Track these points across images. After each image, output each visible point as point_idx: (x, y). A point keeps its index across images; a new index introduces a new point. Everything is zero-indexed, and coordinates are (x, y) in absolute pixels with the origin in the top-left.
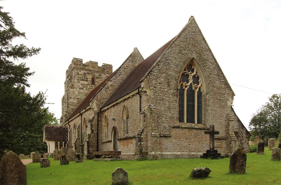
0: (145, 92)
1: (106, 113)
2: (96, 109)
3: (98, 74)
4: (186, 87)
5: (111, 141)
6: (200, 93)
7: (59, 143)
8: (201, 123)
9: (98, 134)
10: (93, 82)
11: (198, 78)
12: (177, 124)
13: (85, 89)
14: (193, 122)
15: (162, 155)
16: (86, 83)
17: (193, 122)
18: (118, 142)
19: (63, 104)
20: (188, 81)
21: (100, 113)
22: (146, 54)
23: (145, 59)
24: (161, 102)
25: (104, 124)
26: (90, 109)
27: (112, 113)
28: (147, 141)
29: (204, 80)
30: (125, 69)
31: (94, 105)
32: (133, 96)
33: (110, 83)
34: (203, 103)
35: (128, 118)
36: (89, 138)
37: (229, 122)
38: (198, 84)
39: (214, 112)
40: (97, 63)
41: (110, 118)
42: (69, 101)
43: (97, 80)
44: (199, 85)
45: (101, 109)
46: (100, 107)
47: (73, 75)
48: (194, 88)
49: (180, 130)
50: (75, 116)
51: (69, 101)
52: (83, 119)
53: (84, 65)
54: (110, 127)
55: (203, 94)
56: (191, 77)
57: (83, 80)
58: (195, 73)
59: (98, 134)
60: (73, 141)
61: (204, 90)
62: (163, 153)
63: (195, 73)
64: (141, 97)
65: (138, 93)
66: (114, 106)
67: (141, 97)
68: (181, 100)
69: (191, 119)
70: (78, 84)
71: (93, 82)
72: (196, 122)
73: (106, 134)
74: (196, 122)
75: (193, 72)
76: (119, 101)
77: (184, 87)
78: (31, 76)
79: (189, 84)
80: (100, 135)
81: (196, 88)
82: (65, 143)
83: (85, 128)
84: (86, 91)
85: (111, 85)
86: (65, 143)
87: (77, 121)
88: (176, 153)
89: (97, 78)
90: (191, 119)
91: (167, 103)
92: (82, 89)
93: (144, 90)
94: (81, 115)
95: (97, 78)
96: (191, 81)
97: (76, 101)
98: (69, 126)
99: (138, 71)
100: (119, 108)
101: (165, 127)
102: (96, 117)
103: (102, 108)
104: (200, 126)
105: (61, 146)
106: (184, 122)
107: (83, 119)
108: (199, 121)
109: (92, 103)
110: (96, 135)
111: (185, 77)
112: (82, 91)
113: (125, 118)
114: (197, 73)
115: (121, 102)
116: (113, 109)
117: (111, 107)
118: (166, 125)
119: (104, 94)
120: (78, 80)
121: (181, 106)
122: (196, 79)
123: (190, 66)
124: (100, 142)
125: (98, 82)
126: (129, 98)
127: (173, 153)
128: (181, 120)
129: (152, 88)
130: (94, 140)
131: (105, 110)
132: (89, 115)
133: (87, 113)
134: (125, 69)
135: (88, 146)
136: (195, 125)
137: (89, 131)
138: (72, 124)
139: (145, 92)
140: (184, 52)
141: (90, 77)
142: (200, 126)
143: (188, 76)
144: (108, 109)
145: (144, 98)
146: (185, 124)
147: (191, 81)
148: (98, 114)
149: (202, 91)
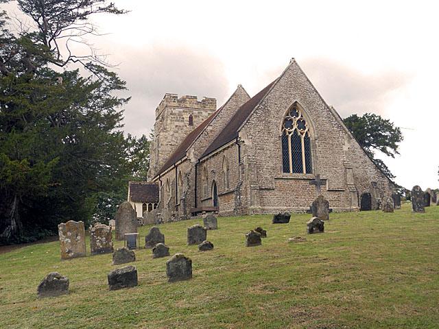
0: (244, 142)
1: (205, 165)
2: (193, 160)
3: (197, 112)
4: (290, 133)
5: (219, 196)
6: (307, 139)
7: (147, 205)
8: (311, 173)
9: (196, 190)
10: (191, 123)
11: (304, 122)
12: (282, 175)
13: (180, 132)
14: (301, 171)
15: (264, 210)
16: (182, 124)
17: (301, 171)
18: (219, 198)
19: (24, 243)
20: (292, 127)
21: (199, 164)
22: (252, 92)
23: (251, 97)
24: (261, 151)
25: (203, 178)
26: (186, 159)
27: (211, 164)
28: (246, 195)
29: (310, 124)
30: (227, 110)
31: (192, 155)
32: (232, 145)
33: (210, 128)
34: (312, 149)
35: (228, 170)
36: (185, 196)
37: (346, 171)
38: (304, 128)
39: (326, 160)
40: (195, 98)
41: (209, 170)
42: (160, 149)
43: (194, 120)
44: (306, 130)
45: (199, 160)
46: (199, 158)
47: (166, 115)
48: (299, 134)
49: (285, 181)
50: (169, 169)
51: (160, 149)
52: (178, 173)
53: (178, 101)
54: (210, 181)
55: (311, 139)
56: (295, 122)
57: (178, 121)
58: (299, 117)
59: (196, 190)
60: (166, 202)
61: (312, 135)
62: (265, 208)
63: (299, 117)
64: (239, 147)
65: (236, 143)
66: (213, 156)
67: (239, 147)
68: (285, 148)
69: (298, 169)
70: (171, 125)
71: (191, 123)
72: (291, 170)
73: (206, 191)
74: (305, 172)
75: (297, 116)
76: (218, 151)
77: (288, 134)
78: (130, 100)
79: (293, 129)
80: (198, 191)
81: (302, 134)
82: (156, 205)
83: (180, 184)
84: (182, 135)
85: (211, 131)
86: (156, 205)
87: (171, 175)
88: (281, 207)
89: (196, 116)
90: (298, 169)
91: (268, 152)
92: (177, 132)
93: (242, 140)
94: (176, 167)
95: (196, 116)
96: (295, 127)
97: (169, 148)
98: (160, 182)
99: (247, 109)
100: (220, 158)
101: (266, 179)
102: (194, 170)
103: (201, 158)
104: (310, 176)
105: (150, 209)
106: (289, 172)
107: (178, 173)
108: (309, 171)
109: (189, 154)
110: (194, 191)
111: (287, 123)
112: (176, 135)
113: (225, 169)
114: (302, 116)
115: (220, 152)
116: (212, 160)
117: (210, 157)
118: (268, 176)
119: (203, 142)
120: (171, 120)
121: (285, 154)
122: (302, 124)
123: (294, 110)
124: (198, 199)
125: (198, 122)
126: (229, 147)
127: (278, 208)
128: (286, 170)
129: (250, 137)
130: (191, 198)
131: (204, 161)
132: (185, 168)
133: (183, 165)
134: (227, 110)
135: (185, 205)
136: (304, 175)
137: (185, 187)
138: (164, 179)
139: (244, 142)
140: (284, 96)
141: (186, 117)
142: (310, 176)
143: (291, 120)
144: (207, 159)
145: (242, 148)
146: (291, 175)
147: (295, 127)
148: (196, 166)
149: (309, 136)
